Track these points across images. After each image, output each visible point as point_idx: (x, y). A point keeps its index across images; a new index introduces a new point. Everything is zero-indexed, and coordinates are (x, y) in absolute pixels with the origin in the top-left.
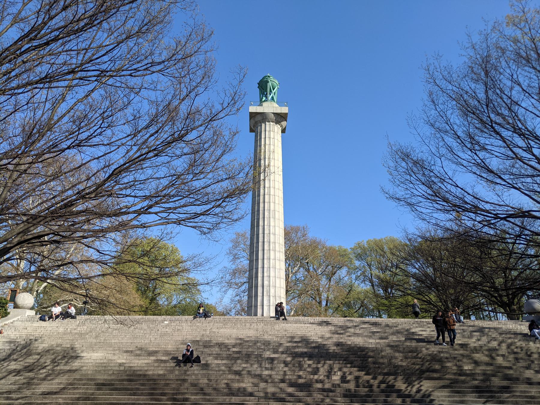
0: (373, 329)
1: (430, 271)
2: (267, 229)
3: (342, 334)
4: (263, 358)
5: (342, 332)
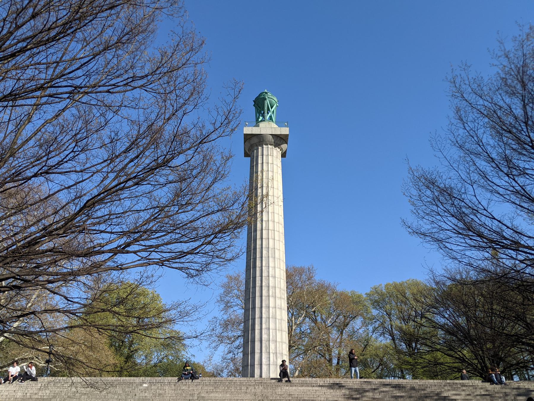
1: (462, 321)
2: (266, 271)
5: (358, 396)
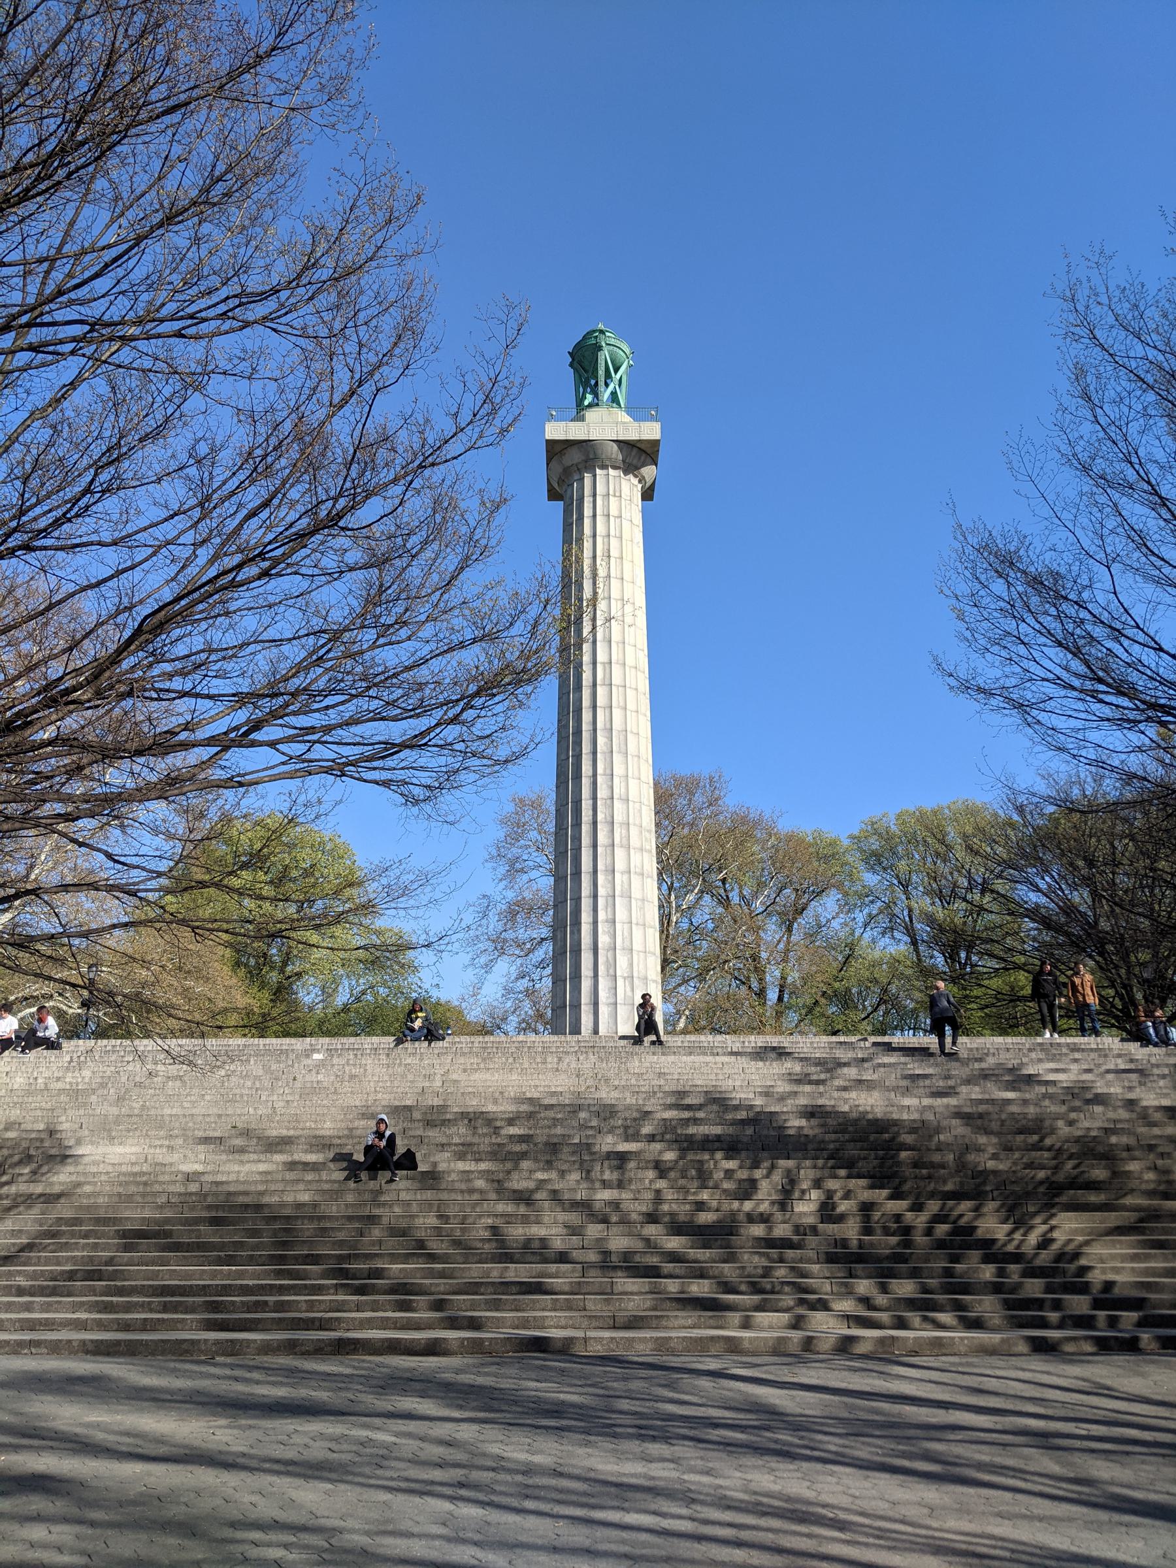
0: (914, 1069)
1: (1080, 897)
2: (604, 786)
3: (818, 1082)
4: (595, 1153)
5: (823, 1076)
